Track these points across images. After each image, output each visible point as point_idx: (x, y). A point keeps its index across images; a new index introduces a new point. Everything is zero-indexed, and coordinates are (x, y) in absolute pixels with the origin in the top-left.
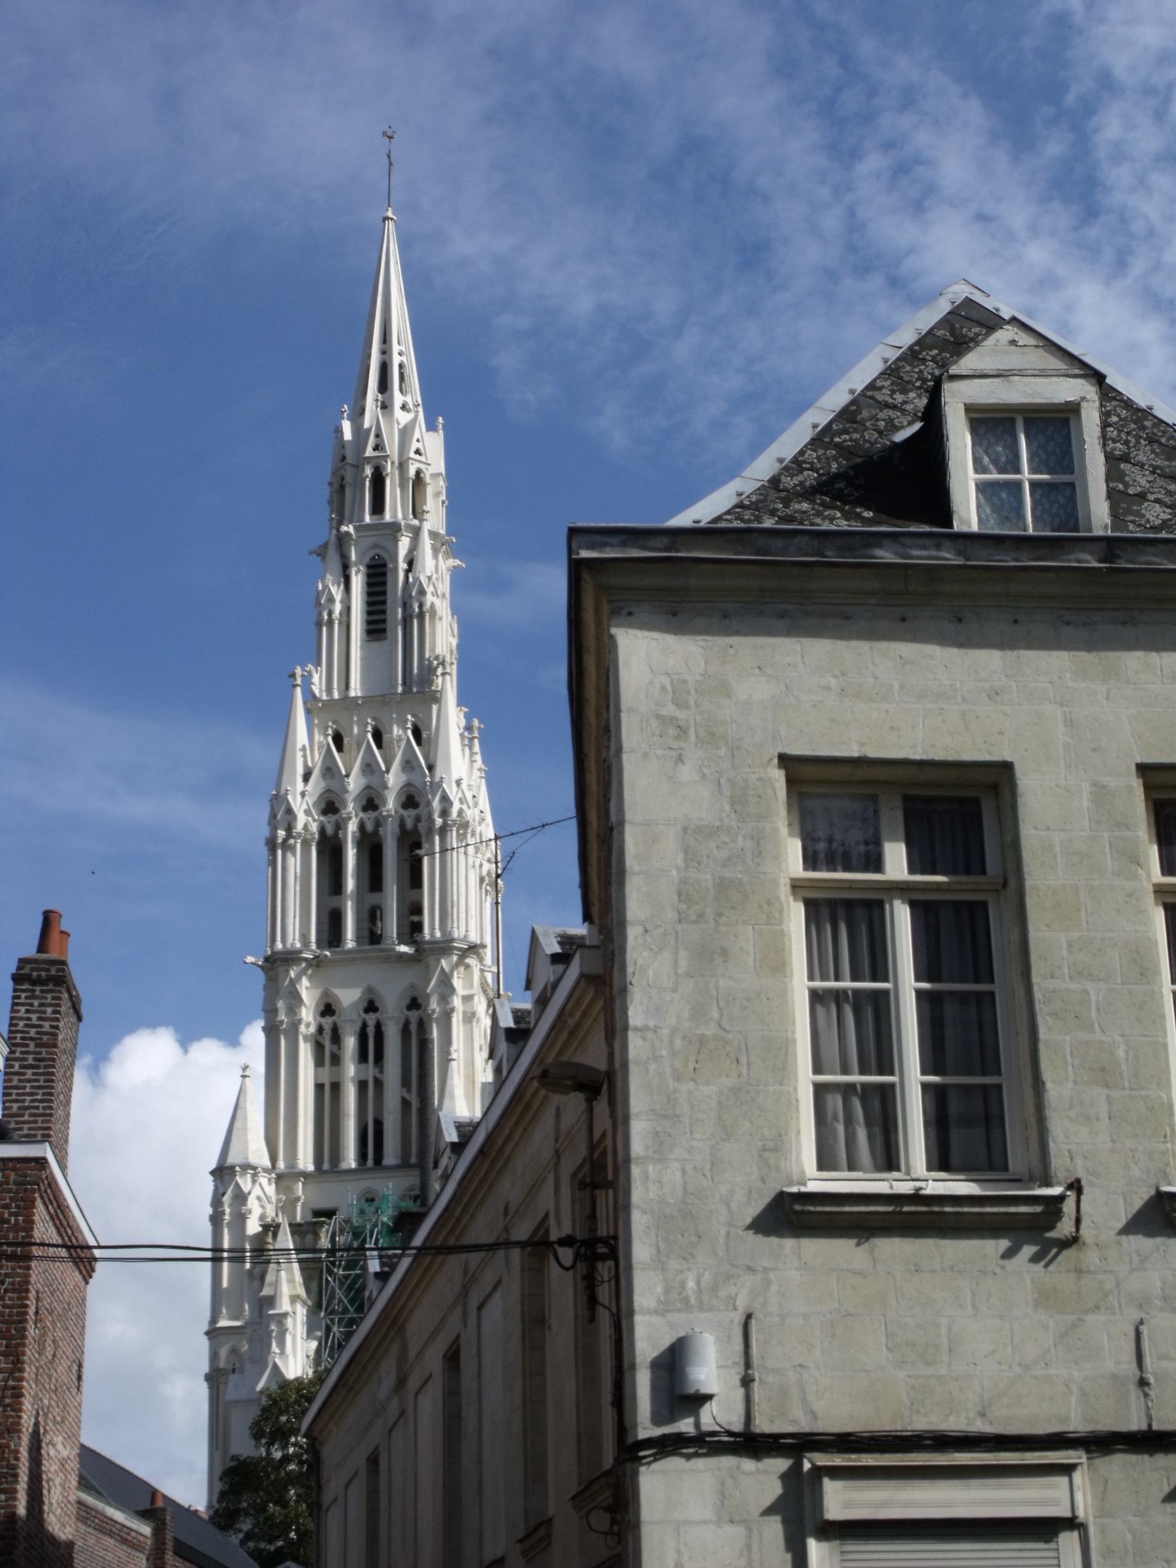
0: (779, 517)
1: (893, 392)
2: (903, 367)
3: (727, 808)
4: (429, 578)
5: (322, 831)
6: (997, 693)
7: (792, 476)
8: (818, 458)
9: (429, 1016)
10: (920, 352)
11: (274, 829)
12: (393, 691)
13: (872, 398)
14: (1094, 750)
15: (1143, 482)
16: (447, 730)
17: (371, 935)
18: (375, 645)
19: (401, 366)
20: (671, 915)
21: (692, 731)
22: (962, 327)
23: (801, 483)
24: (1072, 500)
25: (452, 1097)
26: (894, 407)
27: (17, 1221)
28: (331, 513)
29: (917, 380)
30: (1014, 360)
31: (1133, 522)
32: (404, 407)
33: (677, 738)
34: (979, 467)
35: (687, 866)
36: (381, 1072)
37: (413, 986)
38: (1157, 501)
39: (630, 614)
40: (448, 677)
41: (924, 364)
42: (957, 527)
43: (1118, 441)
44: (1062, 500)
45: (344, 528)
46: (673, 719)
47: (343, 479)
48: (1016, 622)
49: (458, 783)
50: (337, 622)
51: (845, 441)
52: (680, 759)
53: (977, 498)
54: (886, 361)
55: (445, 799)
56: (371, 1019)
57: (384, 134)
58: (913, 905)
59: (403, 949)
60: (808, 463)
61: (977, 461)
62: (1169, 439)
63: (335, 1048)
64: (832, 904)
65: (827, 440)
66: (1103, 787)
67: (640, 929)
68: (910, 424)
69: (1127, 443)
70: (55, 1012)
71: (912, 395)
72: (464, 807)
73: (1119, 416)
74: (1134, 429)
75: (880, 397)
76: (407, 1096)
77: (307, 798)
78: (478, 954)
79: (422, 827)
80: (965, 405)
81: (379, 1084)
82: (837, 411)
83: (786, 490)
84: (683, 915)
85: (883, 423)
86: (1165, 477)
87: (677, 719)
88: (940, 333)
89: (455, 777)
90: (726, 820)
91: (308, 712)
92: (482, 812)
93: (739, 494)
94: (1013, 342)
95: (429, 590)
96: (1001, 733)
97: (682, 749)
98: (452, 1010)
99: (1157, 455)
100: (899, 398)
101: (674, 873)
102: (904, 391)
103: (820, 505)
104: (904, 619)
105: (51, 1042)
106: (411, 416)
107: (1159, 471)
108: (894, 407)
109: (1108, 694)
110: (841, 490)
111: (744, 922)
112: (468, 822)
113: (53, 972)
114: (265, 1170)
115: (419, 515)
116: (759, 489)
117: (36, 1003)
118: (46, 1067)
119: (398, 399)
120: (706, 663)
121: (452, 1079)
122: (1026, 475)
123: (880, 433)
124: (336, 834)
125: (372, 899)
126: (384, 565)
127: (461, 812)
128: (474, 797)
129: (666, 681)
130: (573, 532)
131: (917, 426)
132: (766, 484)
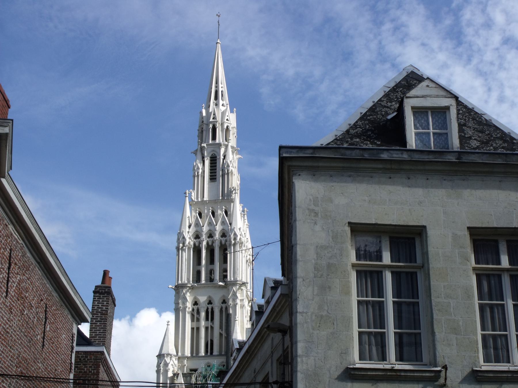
0: (349, 143)
1: (387, 102)
2: (391, 94)
3: (331, 240)
4: (231, 161)
5: (195, 244)
6: (421, 203)
7: (353, 130)
8: (362, 124)
9: (229, 306)
10: (396, 89)
11: (179, 244)
12: (218, 199)
13: (380, 104)
14: (453, 222)
15: (470, 133)
16: (236, 212)
17: (210, 279)
18: (213, 183)
19: (222, 92)
20: (312, 275)
21: (320, 214)
22: (410, 81)
23: (357, 132)
24: (447, 139)
25: (236, 333)
26: (388, 107)
27: (94, 372)
28: (198, 140)
29: (395, 98)
30: (428, 92)
31: (467, 146)
32: (223, 105)
33: (315, 216)
34: (416, 128)
35: (317, 259)
36: (213, 324)
37: (224, 296)
38: (475, 139)
39: (299, 175)
40: (237, 194)
41: (397, 93)
42: (408, 147)
43: (462, 119)
44: (444, 139)
45: (203, 145)
46: (313, 210)
47: (202, 128)
48: (428, 179)
49: (240, 229)
50: (200, 176)
51: (371, 118)
52: (315, 223)
53: (415, 138)
54: (385, 92)
55: (235, 234)
56: (210, 306)
57: (217, 15)
58: (392, 273)
59: (221, 283)
60: (359, 126)
61: (415, 125)
62: (479, 119)
63: (198, 316)
64: (365, 272)
65: (365, 118)
66: (456, 234)
67: (301, 280)
68: (393, 113)
69: (465, 120)
70: (107, 303)
71: (393, 103)
72: (242, 237)
73: (462, 111)
74: (468, 115)
75: (383, 104)
76: (221, 332)
77: (190, 233)
78: (245, 286)
79: (227, 243)
80: (411, 107)
81: (212, 328)
82: (369, 108)
83: (352, 135)
84: (316, 275)
85: (384, 113)
86: (478, 131)
87: (315, 210)
88: (403, 83)
89: (238, 227)
90: (330, 244)
91: (190, 205)
92: (247, 239)
93: (336, 136)
94: (428, 86)
95: (231, 165)
96: (422, 216)
97: (316, 220)
98: (237, 304)
99: (475, 124)
100: (389, 104)
101: (313, 261)
102: (391, 102)
103: (363, 139)
104: (390, 178)
105: (106, 313)
106: (225, 108)
107: (476, 129)
108: (388, 107)
109: (458, 204)
110: (370, 135)
111: (336, 278)
112: (243, 242)
113: (107, 290)
114: (174, 356)
115: (227, 141)
116: (342, 134)
117: (101, 300)
118: (104, 321)
119: (221, 102)
120: (325, 191)
121: (236, 327)
122: (431, 130)
123: (383, 116)
124: (199, 245)
125: (211, 267)
126: (216, 157)
127: (240, 239)
128: (245, 234)
129: (311, 198)
130: (281, 148)
131: (395, 114)
132: (345, 132)
